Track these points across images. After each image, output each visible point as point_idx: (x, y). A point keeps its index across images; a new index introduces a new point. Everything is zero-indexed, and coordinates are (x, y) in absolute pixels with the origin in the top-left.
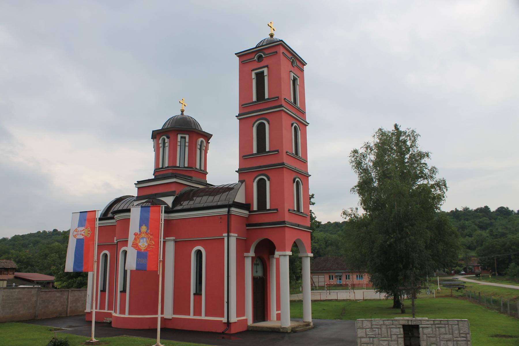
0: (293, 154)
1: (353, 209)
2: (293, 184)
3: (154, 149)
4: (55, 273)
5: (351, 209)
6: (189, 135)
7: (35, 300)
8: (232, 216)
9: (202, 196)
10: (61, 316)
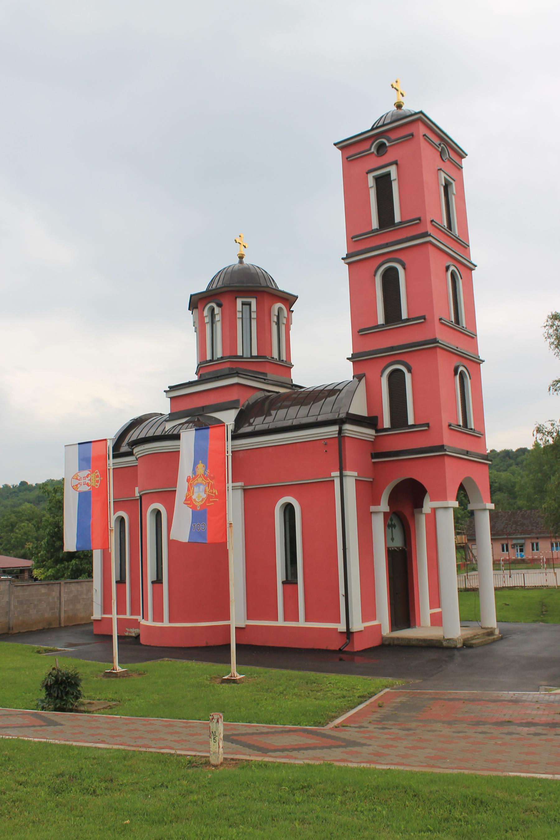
0: (452, 322)
1: (555, 422)
2: (454, 377)
3: (194, 327)
4: (32, 555)
5: (551, 422)
6: (256, 298)
7: (7, 602)
8: (347, 440)
9: (288, 407)
10: (52, 627)
